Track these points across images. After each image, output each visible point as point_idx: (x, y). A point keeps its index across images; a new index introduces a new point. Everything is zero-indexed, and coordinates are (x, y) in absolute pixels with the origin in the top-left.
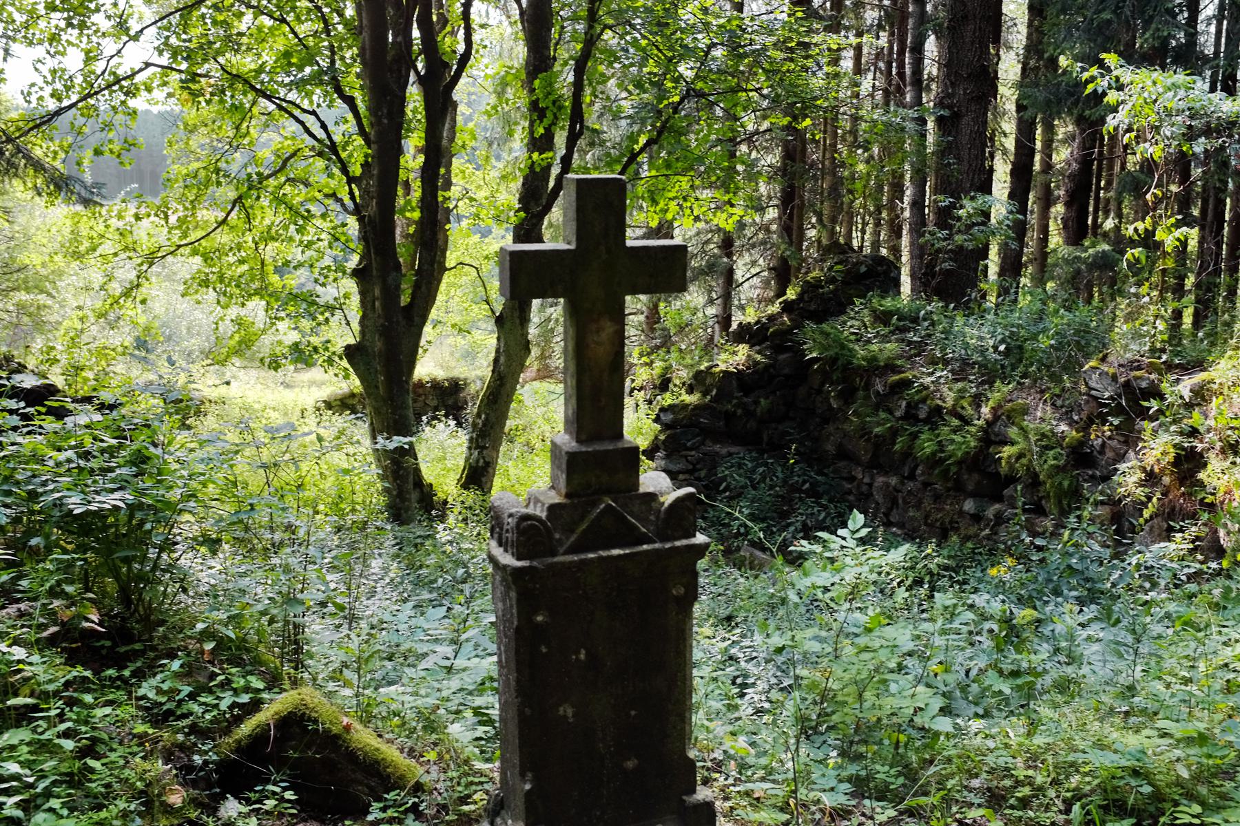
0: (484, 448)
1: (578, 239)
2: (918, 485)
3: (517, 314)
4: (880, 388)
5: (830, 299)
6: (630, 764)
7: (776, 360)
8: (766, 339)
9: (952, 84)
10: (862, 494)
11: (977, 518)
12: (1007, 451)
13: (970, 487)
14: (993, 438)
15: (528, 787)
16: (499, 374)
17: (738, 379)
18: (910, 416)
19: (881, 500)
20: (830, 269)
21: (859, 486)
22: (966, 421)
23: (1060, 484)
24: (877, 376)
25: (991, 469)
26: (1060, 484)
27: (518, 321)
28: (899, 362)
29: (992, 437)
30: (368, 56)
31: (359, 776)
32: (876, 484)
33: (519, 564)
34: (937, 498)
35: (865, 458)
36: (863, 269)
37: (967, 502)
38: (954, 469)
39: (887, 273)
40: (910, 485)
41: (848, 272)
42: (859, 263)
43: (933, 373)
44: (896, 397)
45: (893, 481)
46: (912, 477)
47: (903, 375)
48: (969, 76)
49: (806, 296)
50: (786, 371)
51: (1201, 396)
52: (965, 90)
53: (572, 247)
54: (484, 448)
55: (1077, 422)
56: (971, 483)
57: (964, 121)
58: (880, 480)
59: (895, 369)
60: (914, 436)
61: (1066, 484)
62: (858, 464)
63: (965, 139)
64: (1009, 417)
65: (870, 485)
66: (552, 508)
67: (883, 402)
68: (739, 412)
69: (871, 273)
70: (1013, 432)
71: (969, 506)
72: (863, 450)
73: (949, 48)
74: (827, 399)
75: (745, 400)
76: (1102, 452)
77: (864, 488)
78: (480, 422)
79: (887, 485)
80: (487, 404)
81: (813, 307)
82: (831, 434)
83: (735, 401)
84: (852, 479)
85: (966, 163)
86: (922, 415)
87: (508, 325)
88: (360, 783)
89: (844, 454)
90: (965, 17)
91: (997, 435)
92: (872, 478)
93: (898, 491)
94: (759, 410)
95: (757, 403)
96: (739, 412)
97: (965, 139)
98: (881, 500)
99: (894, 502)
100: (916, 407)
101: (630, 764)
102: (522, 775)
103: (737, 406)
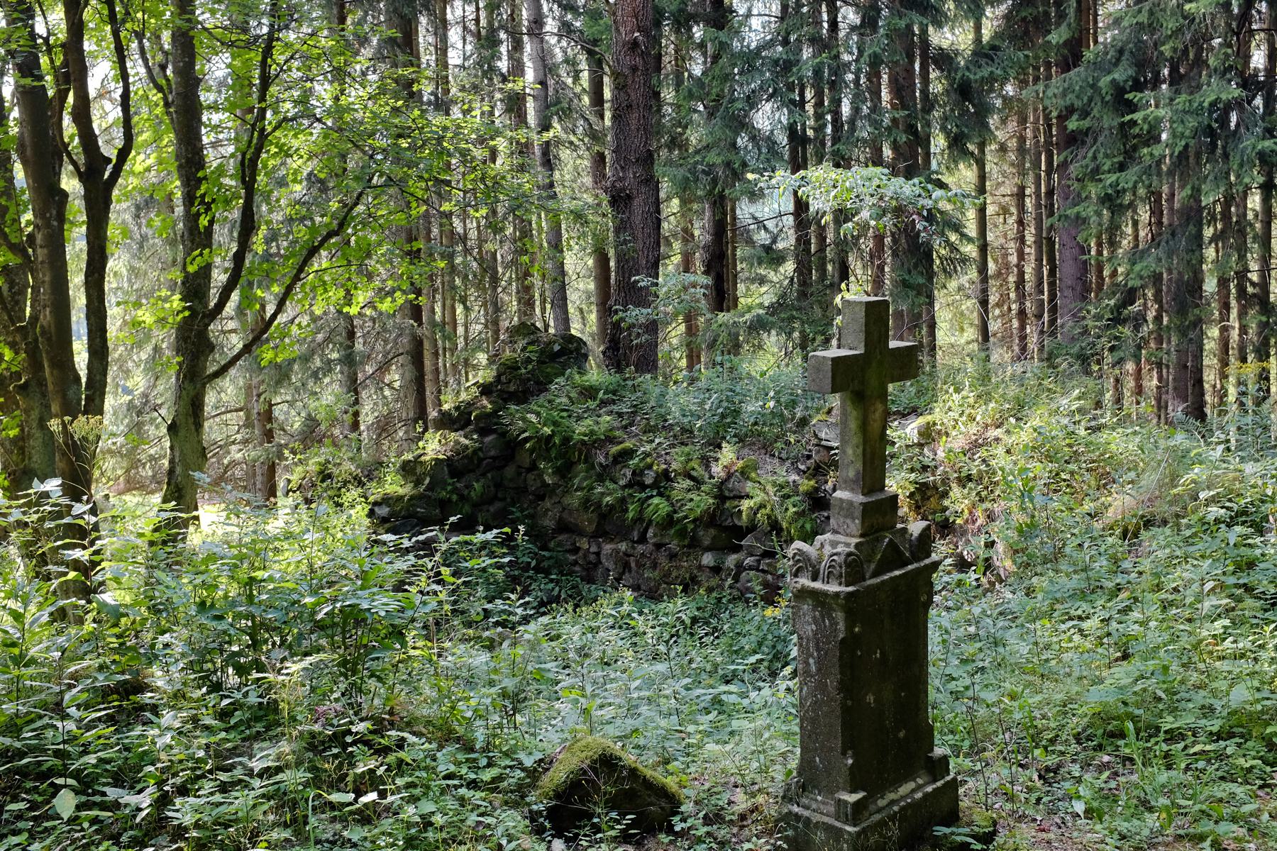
1: (866, 346)
2: (651, 547)
3: (191, 420)
4: (601, 459)
5: (529, 380)
6: (902, 734)
7: (482, 443)
8: (468, 422)
9: (622, 168)
10: (590, 563)
11: (716, 570)
12: (746, 505)
13: (707, 542)
14: (727, 494)
15: (850, 761)
16: (177, 486)
17: (448, 466)
18: (637, 482)
19: (611, 566)
20: (524, 349)
21: (585, 556)
22: (698, 482)
23: (803, 526)
25: (728, 522)
27: (193, 428)
28: (617, 433)
30: (29, 152)
31: (653, 799)
32: (604, 552)
33: (850, 589)
34: (672, 556)
35: (590, 528)
36: (557, 348)
37: (705, 556)
38: (691, 526)
39: (578, 350)
40: (640, 548)
41: (542, 352)
43: (653, 441)
44: (618, 467)
45: (623, 546)
46: (643, 539)
49: (503, 378)
50: (492, 453)
51: (929, 435)
52: (634, 173)
53: (860, 351)
55: (804, 472)
56: (706, 537)
57: (635, 202)
58: (608, 548)
59: (611, 440)
60: (643, 502)
62: (581, 533)
63: (637, 220)
64: (742, 473)
65: (598, 554)
66: (857, 546)
67: (604, 475)
68: (455, 497)
69: (562, 352)
70: (749, 487)
71: (708, 559)
72: (587, 522)
74: (540, 476)
75: (458, 485)
77: (592, 558)
79: (617, 551)
81: (512, 388)
82: (548, 510)
83: (449, 488)
84: (576, 550)
85: (640, 241)
86: (648, 481)
87: (182, 433)
88: (653, 805)
89: (564, 527)
90: (630, 106)
91: (730, 491)
92: (599, 547)
93: (629, 556)
94: (473, 494)
95: (469, 487)
96: (455, 497)
97: (637, 220)
98: (611, 566)
99: (626, 566)
100: (642, 472)
101: (902, 734)
103: (452, 492)
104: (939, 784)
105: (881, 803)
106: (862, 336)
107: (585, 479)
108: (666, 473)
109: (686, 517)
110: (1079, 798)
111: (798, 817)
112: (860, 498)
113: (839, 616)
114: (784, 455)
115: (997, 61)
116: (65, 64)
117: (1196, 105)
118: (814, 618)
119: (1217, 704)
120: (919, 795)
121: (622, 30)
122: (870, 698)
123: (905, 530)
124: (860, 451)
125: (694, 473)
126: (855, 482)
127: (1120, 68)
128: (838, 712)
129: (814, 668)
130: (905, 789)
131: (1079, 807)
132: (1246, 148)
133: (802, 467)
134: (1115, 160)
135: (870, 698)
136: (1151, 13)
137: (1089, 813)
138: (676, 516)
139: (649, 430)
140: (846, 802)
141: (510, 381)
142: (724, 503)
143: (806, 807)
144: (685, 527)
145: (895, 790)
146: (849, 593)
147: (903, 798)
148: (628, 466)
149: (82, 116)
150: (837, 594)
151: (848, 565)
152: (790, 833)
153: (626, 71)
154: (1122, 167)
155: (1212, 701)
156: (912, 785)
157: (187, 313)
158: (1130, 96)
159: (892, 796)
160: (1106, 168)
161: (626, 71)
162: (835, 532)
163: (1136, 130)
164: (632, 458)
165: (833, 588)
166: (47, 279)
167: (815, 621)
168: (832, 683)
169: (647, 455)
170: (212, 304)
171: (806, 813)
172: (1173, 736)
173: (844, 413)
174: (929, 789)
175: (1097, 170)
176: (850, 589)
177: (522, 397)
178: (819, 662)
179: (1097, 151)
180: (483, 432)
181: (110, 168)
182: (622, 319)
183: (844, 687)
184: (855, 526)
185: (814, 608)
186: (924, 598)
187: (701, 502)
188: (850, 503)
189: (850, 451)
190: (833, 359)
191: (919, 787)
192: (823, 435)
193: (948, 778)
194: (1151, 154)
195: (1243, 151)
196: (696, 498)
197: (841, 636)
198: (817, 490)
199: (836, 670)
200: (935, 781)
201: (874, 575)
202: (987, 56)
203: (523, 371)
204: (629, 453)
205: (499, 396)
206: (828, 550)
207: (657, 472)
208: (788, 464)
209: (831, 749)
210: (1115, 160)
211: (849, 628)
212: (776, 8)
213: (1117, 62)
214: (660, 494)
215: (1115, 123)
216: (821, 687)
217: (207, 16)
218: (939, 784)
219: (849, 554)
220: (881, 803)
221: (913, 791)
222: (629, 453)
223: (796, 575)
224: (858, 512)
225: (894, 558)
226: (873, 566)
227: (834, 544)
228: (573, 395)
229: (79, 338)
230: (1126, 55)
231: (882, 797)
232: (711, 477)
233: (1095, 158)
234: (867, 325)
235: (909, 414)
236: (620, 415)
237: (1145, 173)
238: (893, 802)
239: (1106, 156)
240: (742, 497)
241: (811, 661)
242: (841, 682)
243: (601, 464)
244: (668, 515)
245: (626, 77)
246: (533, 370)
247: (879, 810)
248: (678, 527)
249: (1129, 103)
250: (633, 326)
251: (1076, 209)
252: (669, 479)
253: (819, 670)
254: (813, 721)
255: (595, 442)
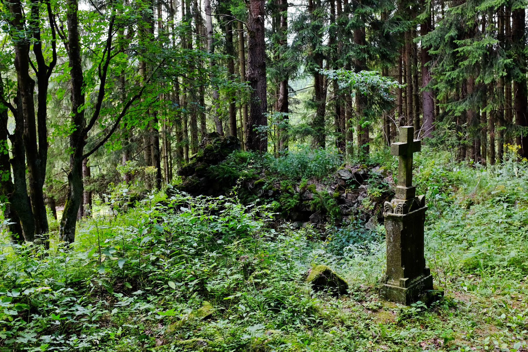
0: (69, 233)
5: (218, 155)
9: (253, 69)
13: (295, 218)
14: (303, 198)
15: (404, 269)
16: (72, 200)
20: (215, 143)
22: (292, 195)
23: (335, 210)
24: (248, 182)
26: (335, 210)
29: (302, 197)
33: (405, 215)
36: (228, 142)
38: (289, 212)
42: (225, 140)
47: (259, 181)
48: (259, 66)
50: (204, 185)
52: (258, 72)
53: (406, 143)
54: (69, 233)
55: (334, 190)
57: (259, 83)
59: (255, 179)
61: (337, 210)
64: (310, 190)
66: (405, 202)
69: (231, 143)
73: (251, 56)
76: (346, 198)
78: (65, 222)
80: (67, 214)
81: (211, 158)
86: (270, 194)
90: (256, 45)
91: (305, 197)
97: (259, 90)
102: (402, 266)
104: (428, 277)
105: (412, 282)
106: (406, 138)
107: (244, 194)
108: (277, 191)
109: (287, 208)
110: (465, 286)
111: (387, 287)
112: (405, 188)
113: (401, 224)
114: (326, 183)
115: (400, 25)
117: (481, 45)
118: (392, 225)
119: (506, 257)
120: (422, 280)
121: (253, 14)
122: (409, 249)
123: (417, 198)
124: (405, 173)
125: (290, 191)
126: (404, 183)
127: (452, 30)
128: (400, 253)
129: (392, 240)
131: (465, 288)
132: (500, 62)
133: (333, 188)
134: (451, 66)
135: (409, 249)
136: (462, 10)
137: (469, 290)
138: (283, 208)
139: (269, 174)
140: (403, 281)
141: (210, 155)
142: (302, 202)
143: (390, 284)
144: (286, 212)
145: (416, 278)
146: (404, 216)
147: (418, 281)
148: (262, 189)
149: (38, 49)
150: (401, 216)
152: (384, 292)
153: (255, 31)
154: (453, 69)
155: (504, 257)
156: (420, 277)
157: (76, 129)
158: (455, 41)
159: (415, 280)
160: (447, 70)
161: (255, 31)
162: (397, 198)
163: (459, 55)
164: (263, 186)
165: (399, 215)
166: (26, 116)
167: (393, 225)
168: (398, 244)
169: (269, 184)
170: (87, 126)
171: (390, 286)
172: (493, 268)
173: (400, 162)
174: (425, 278)
175: (443, 70)
176: (405, 215)
177: (215, 162)
178: (394, 238)
179: (444, 63)
180: (200, 176)
182: (257, 130)
183: (402, 245)
184: (404, 196)
185: (392, 221)
186: (423, 219)
187: (293, 202)
188: (403, 189)
189: (402, 173)
190: (400, 145)
191: (422, 278)
192: (342, 175)
194: (464, 65)
195: (499, 64)
196: (291, 201)
197: (402, 229)
198: (340, 196)
199: (400, 240)
202: (396, 23)
203: (215, 151)
204: (262, 184)
205: (205, 162)
206: (396, 204)
207: (274, 191)
208: (328, 186)
209: (398, 265)
210: (451, 66)
211: (404, 227)
212: (307, 3)
213: (450, 28)
214: (275, 200)
215: (451, 52)
216: (395, 246)
217: (84, 7)
218: (428, 277)
219: (404, 204)
220: (412, 282)
221: (421, 279)
222: (262, 184)
223: (386, 212)
224: (405, 192)
225: (415, 206)
226: (410, 208)
227: (398, 202)
228: (237, 161)
230: (453, 26)
232: (297, 192)
233: (443, 65)
234: (408, 134)
235: (376, 166)
236: (256, 168)
237: (461, 72)
238: (415, 282)
239: (447, 65)
240: (310, 200)
241: (391, 238)
242: (401, 244)
243: (250, 188)
244: (279, 207)
245: (255, 33)
246: (219, 151)
247: (412, 284)
248: (283, 212)
249: (455, 44)
250: (260, 133)
251: (436, 86)
252: (279, 194)
253: (394, 241)
254: (391, 257)
255: (248, 179)
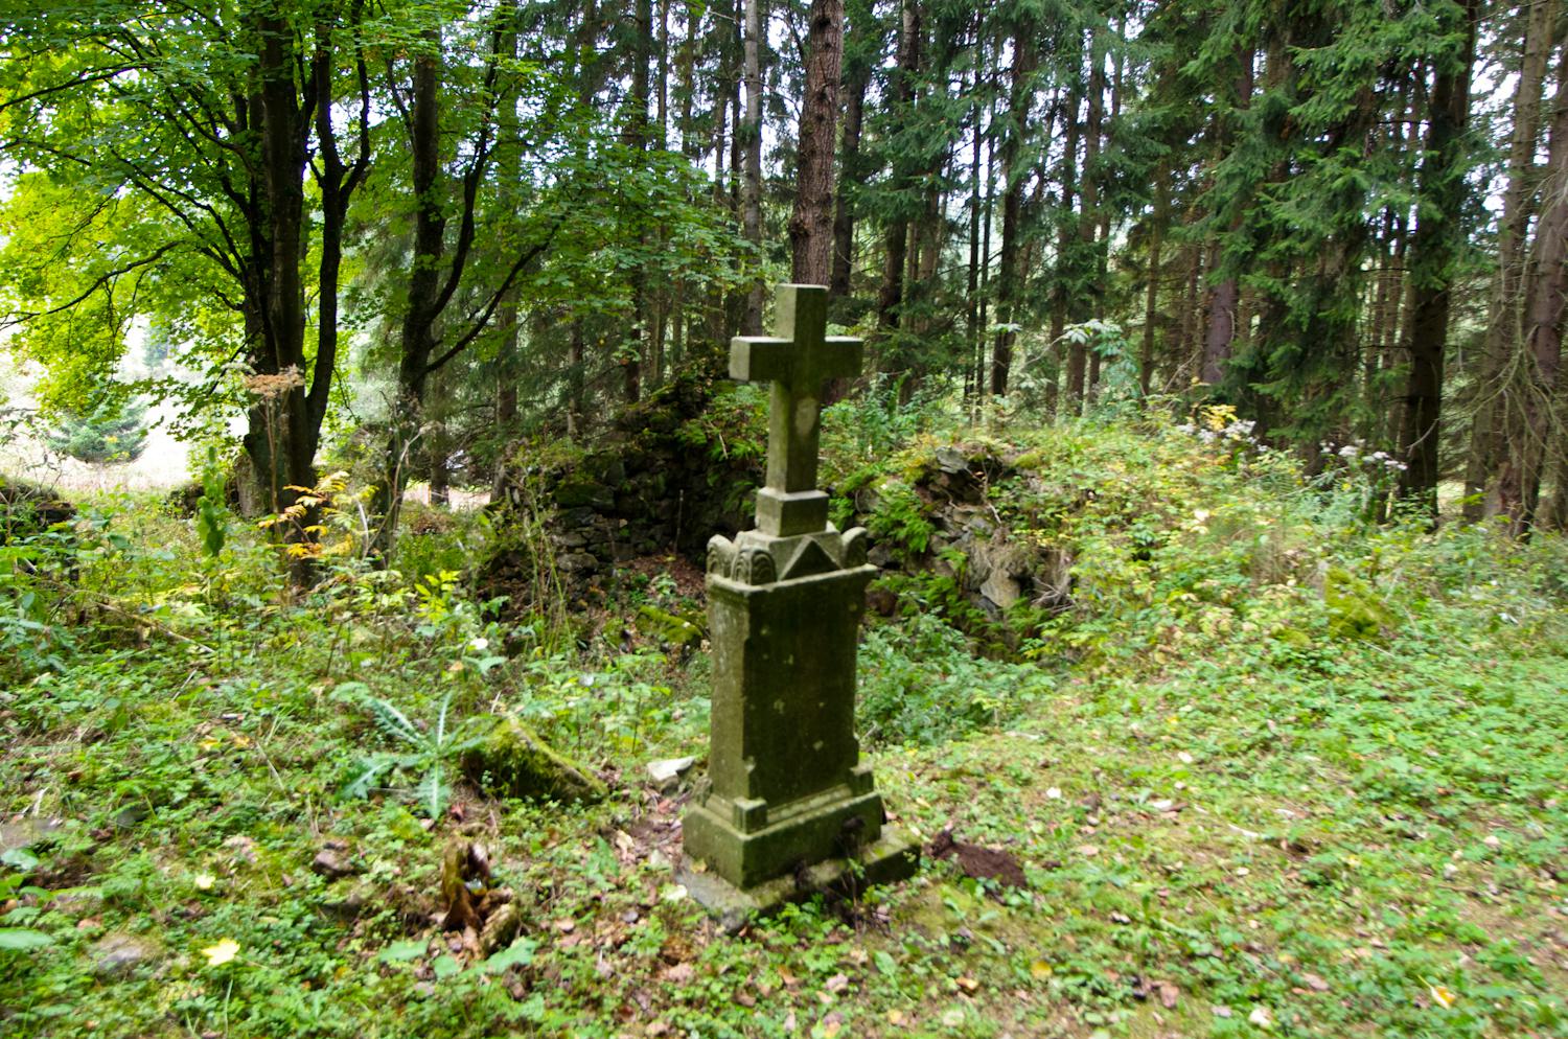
6: (818, 745)
33: (757, 588)
53: (790, 339)
57: (812, 241)
101: (818, 745)
116: (313, 80)
130: (817, 801)
140: (741, 810)
151: (755, 564)
174: (845, 804)
176: (757, 588)
181: (347, 175)
183: (747, 689)
193: (871, 795)
200: (855, 795)
201: (789, 576)
218: (858, 800)
229: (312, 332)
231: (789, 807)
234: (798, 311)
238: (800, 813)
